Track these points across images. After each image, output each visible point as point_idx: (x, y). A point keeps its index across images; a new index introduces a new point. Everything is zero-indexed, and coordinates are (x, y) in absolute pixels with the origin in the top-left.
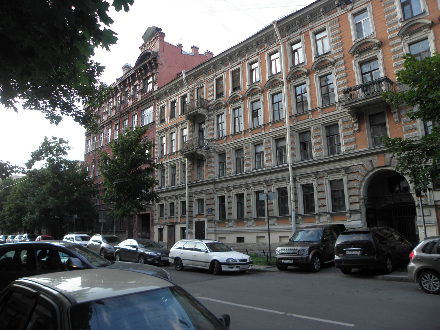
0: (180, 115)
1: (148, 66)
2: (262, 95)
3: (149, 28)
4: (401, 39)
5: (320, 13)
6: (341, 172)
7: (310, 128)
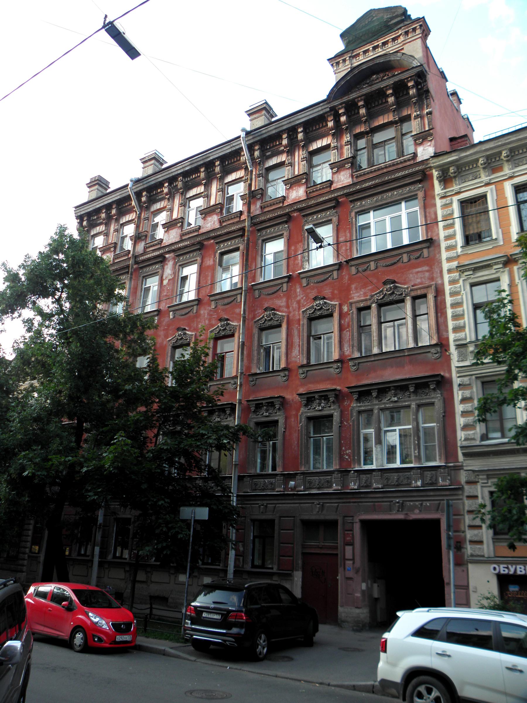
1: (359, 108)
3: (370, 13)
4: (460, 275)
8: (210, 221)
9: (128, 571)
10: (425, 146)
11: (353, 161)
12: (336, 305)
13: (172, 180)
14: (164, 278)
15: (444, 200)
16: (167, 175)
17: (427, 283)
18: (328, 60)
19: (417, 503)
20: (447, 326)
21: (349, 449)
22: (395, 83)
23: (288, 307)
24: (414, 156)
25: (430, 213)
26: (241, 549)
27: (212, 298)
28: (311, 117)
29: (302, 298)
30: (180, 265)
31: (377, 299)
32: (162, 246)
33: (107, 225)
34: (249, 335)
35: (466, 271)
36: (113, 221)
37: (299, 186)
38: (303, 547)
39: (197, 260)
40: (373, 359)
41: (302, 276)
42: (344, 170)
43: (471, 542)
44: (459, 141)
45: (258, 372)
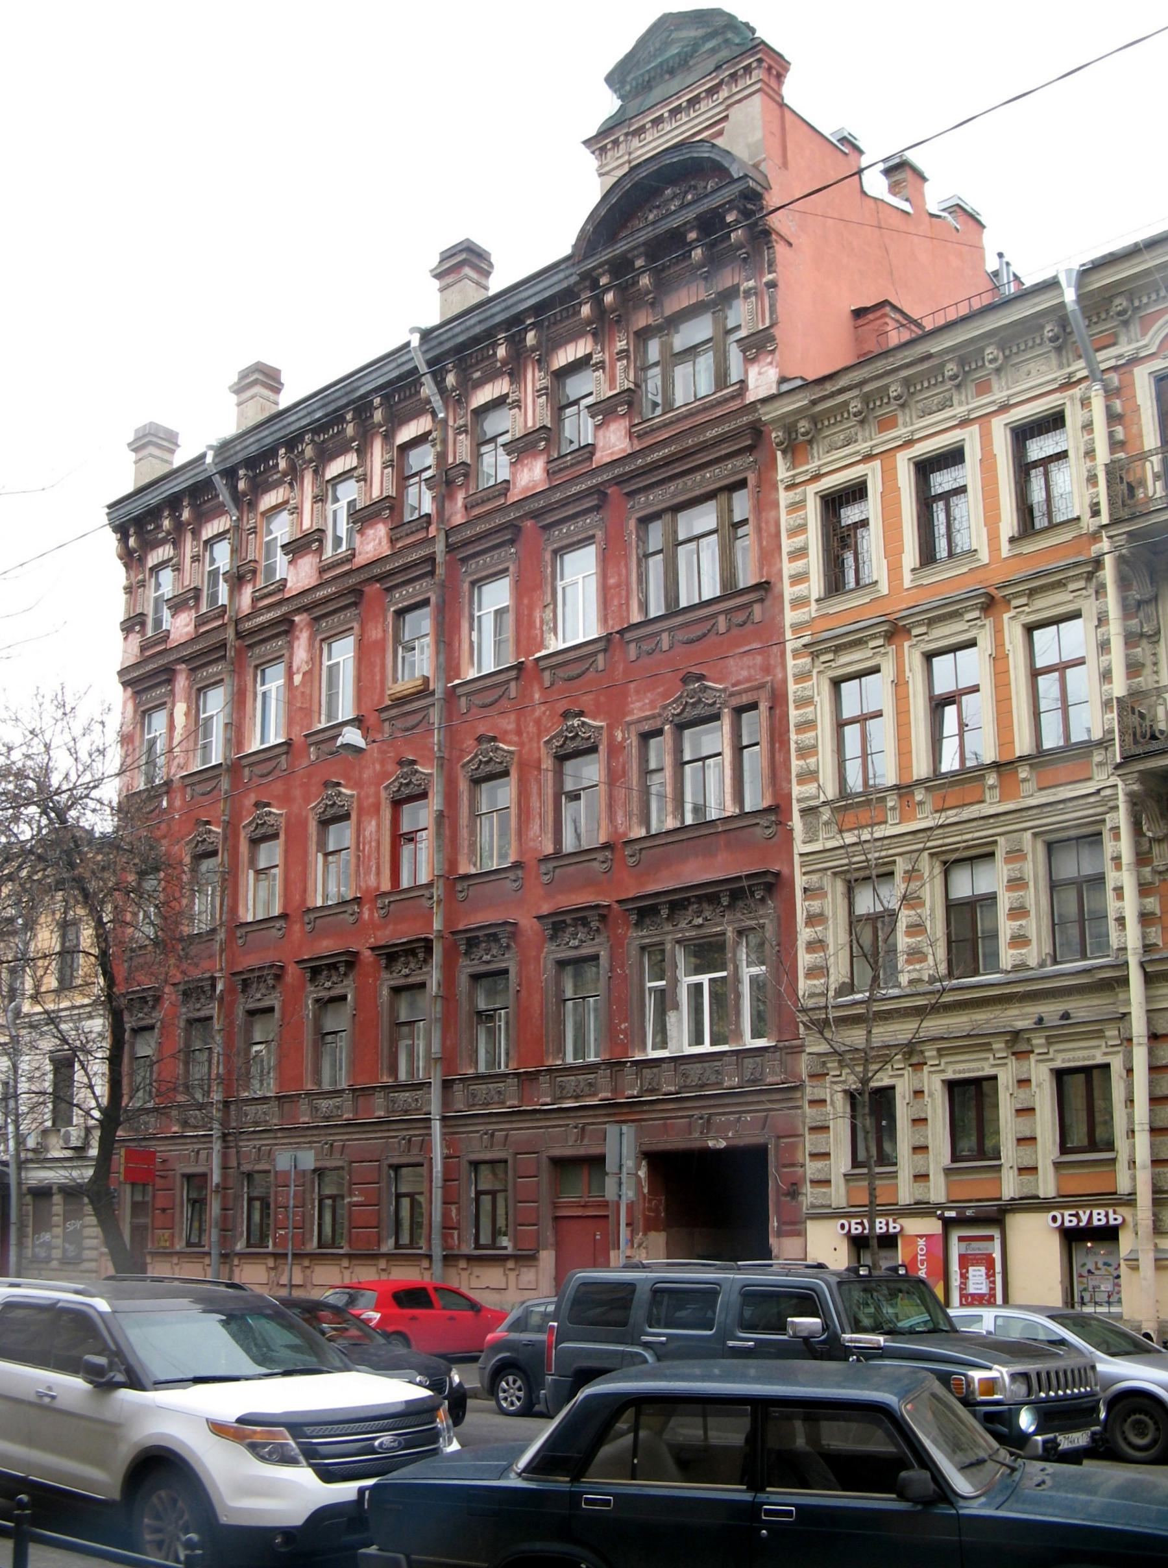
0: (1012, 540)
2: (987, 622)
5: (983, 365)
6: (1104, 1037)
7: (995, 842)
8: (372, 536)
9: (272, 1269)
10: (762, 364)
11: (630, 399)
12: (602, 727)
13: (292, 443)
14: (295, 668)
15: (791, 494)
16: (280, 429)
17: (760, 678)
18: (586, 142)
19: (732, 1118)
20: (789, 771)
21: (626, 1020)
22: (699, 217)
23: (519, 733)
24: (741, 388)
25: (767, 522)
27: (384, 715)
28: (547, 294)
29: (544, 713)
30: (323, 640)
31: (673, 715)
32: (287, 596)
33: (177, 544)
34: (451, 798)
35: (823, 654)
36: (189, 536)
37: (535, 456)
38: (555, 1206)
39: (352, 628)
40: (663, 841)
41: (542, 664)
42: (615, 420)
43: (812, 1182)
44: (871, 316)
45: (473, 871)
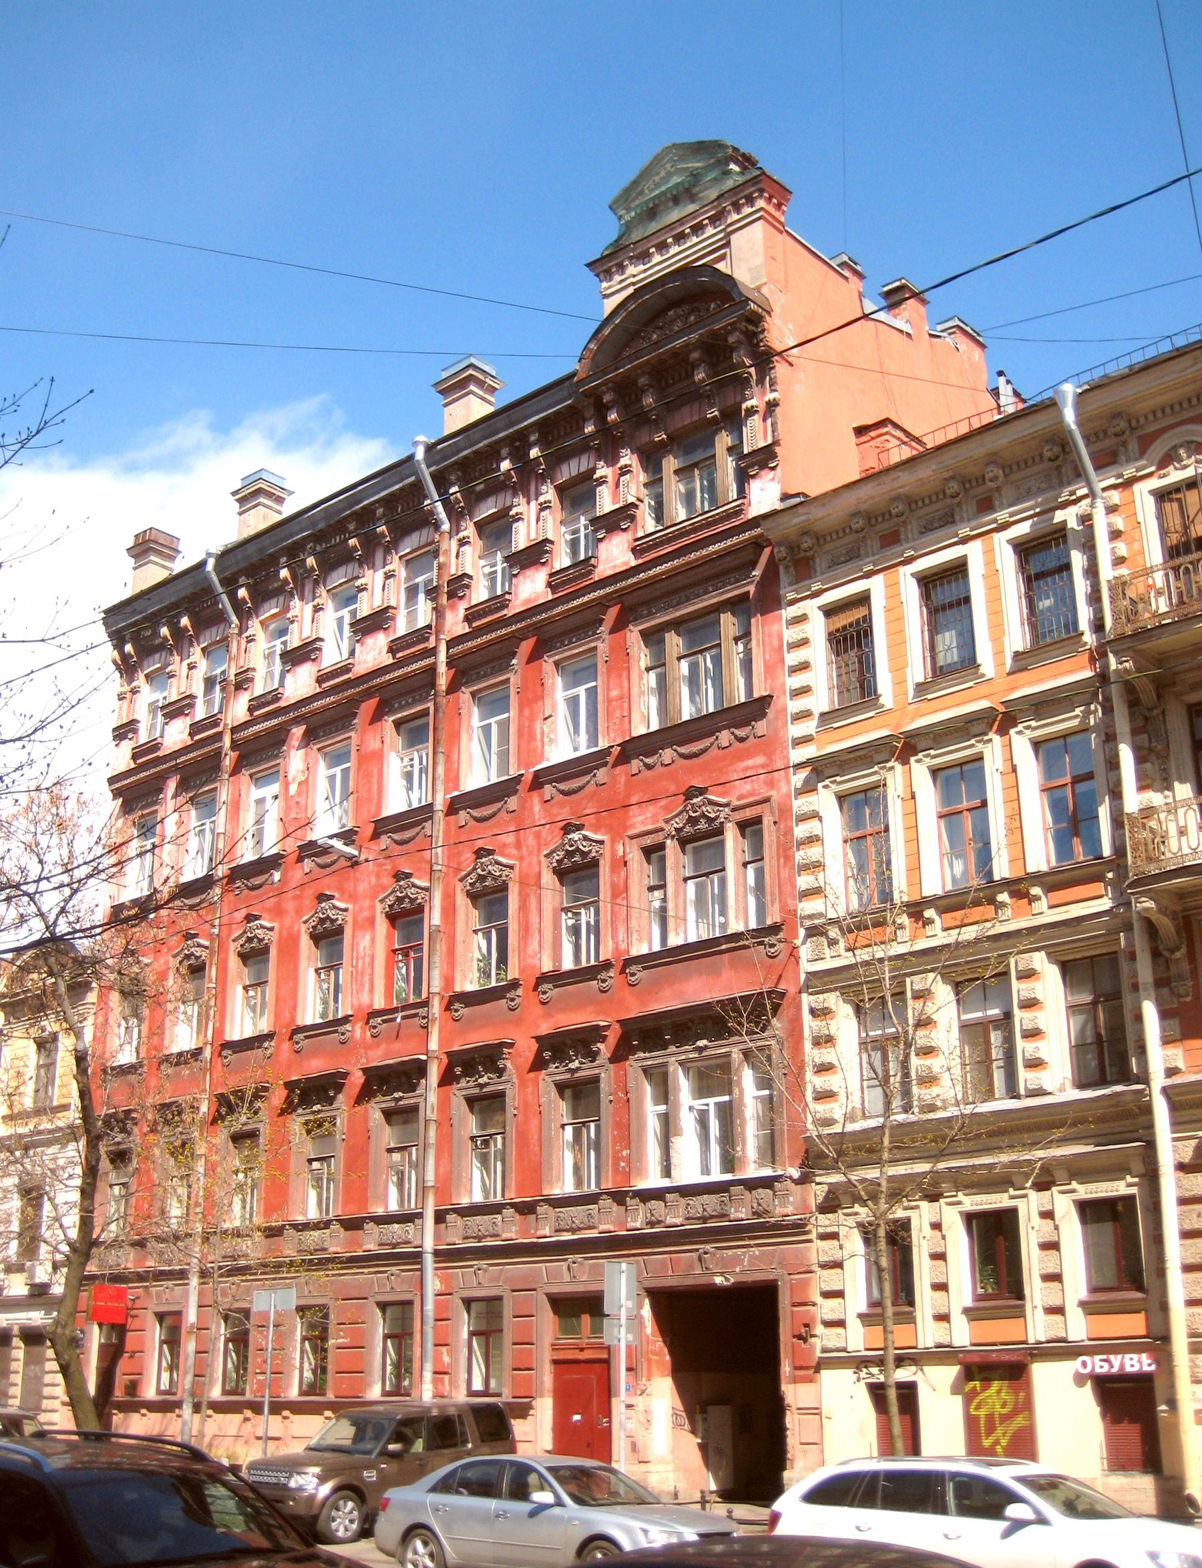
14: (290, 779)
18: (589, 265)
26: (446, 1359)
